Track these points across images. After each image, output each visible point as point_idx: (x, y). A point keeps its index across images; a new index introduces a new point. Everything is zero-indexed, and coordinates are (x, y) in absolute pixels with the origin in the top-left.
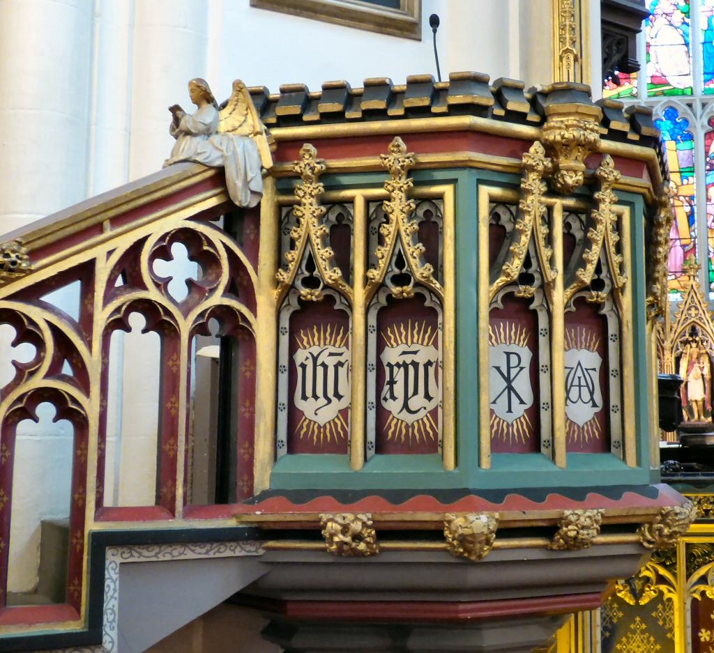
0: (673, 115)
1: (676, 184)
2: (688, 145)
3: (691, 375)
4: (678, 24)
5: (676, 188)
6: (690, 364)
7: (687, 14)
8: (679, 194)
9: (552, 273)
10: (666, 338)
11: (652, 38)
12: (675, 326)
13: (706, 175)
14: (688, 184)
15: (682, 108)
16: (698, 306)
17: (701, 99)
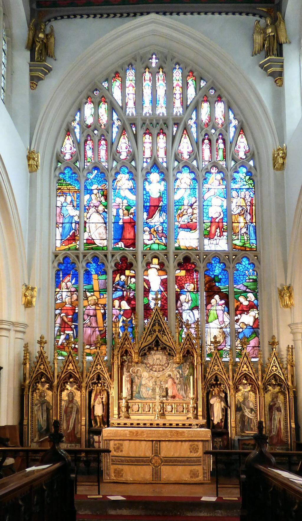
0: (96, 260)
1: (97, 298)
2: (104, 277)
3: (96, 402)
4: (101, 212)
6: (96, 396)
7: (106, 207)
8: (99, 303)
10: (83, 381)
11: (87, 219)
12: (32, 374)
13: (113, 294)
14: (103, 298)
15: (101, 256)
16: (101, 364)
17: (82, 253)
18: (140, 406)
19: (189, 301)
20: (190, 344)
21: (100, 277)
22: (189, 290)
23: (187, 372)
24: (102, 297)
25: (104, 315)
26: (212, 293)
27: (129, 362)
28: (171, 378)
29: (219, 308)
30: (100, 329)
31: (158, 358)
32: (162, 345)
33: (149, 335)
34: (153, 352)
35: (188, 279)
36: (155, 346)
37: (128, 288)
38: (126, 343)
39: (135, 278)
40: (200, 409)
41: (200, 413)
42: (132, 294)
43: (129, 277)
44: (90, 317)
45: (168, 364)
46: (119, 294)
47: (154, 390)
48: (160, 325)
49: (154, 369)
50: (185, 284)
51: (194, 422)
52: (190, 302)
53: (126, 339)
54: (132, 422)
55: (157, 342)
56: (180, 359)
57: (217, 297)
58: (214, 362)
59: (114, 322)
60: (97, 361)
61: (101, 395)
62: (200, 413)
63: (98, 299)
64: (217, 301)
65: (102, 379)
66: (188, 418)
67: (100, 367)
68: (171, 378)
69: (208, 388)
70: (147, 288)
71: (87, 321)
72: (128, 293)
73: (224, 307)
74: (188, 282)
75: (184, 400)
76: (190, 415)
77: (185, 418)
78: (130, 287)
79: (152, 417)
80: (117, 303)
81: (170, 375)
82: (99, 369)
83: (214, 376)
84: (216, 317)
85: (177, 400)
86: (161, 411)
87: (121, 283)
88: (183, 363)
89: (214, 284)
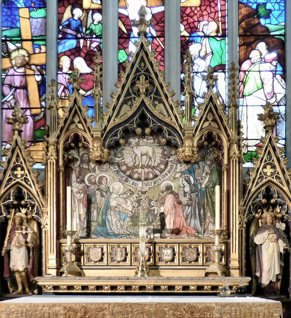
1: (28, 52)
2: (41, 13)
3: (13, 243)
5: (28, 57)
13: (58, 44)
14: (40, 53)
16: (24, 166)
18: (105, 250)
19: (206, 54)
20: (214, 120)
21: (34, 14)
22: (207, 33)
23: (207, 180)
24: (37, 50)
25: (42, 86)
26: (252, 39)
27: (82, 162)
28: (172, 193)
29: (267, 66)
30: (34, 111)
31: (144, 152)
32: (154, 123)
33: (125, 102)
34: (133, 141)
35: (205, 13)
36: (139, 126)
37: (88, 32)
38: (76, 120)
39: (101, 13)
40: (234, 255)
41: (234, 263)
42: (94, 45)
43: (91, 12)
44: (15, 91)
45: (166, 165)
46: (71, 44)
47: (135, 219)
48: (148, 78)
49: (136, 176)
50: (199, 22)
51: (224, 282)
52: (209, 58)
53: (76, 110)
54: (85, 283)
55: (143, 117)
56: (193, 152)
57: (262, 46)
58: (265, 158)
59: (61, 99)
60: (14, 159)
61: (22, 229)
62: (234, 263)
63: (29, 56)
64: (261, 54)
65: (26, 197)
66: (207, 274)
67: (23, 172)
68: (172, 193)
69: (250, 212)
70: (125, 31)
71: (9, 98)
72: (89, 42)
73: (276, 66)
74: (206, 18)
75: (199, 238)
76: (214, 267)
77: (202, 273)
78: (92, 31)
79: (131, 273)
80: (65, 61)
81: (169, 188)
82: (19, 176)
83: (264, 188)
84: (260, 85)
85: (184, 238)
86: (149, 260)
87: (74, 24)
88: (197, 163)
89: (256, 22)
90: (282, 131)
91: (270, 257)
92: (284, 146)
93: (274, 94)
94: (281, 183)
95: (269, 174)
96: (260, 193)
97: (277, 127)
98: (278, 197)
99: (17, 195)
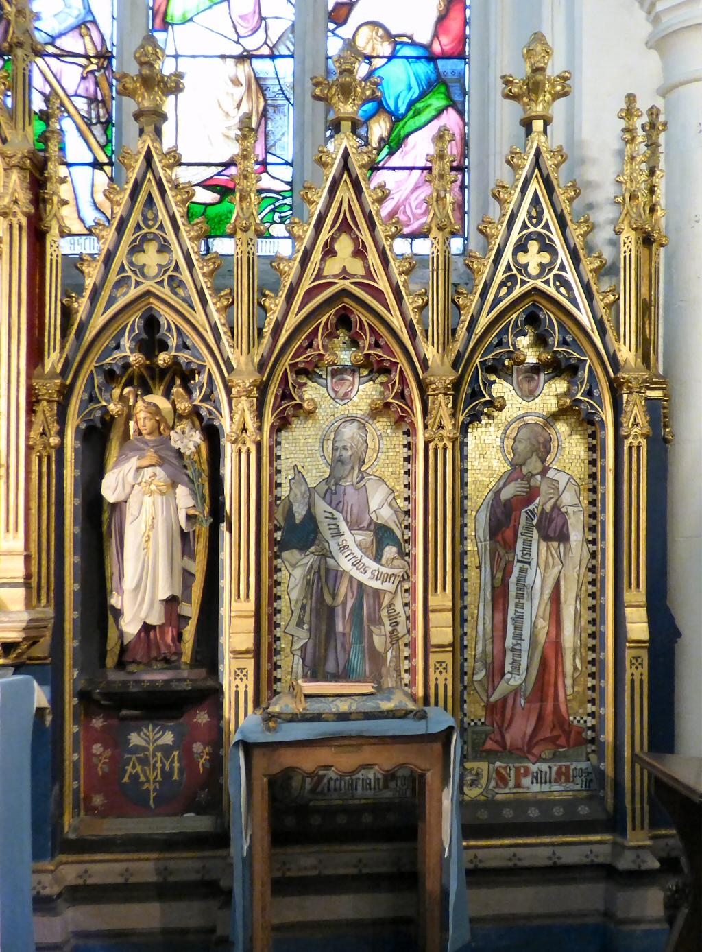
9: (15, 206)
90: (285, 139)
91: (141, 541)
92: (288, 188)
93: (261, 18)
94: (574, 301)
95: (533, 270)
96: (314, 333)
97: (270, 127)
98: (377, 345)
99: (144, 336)
